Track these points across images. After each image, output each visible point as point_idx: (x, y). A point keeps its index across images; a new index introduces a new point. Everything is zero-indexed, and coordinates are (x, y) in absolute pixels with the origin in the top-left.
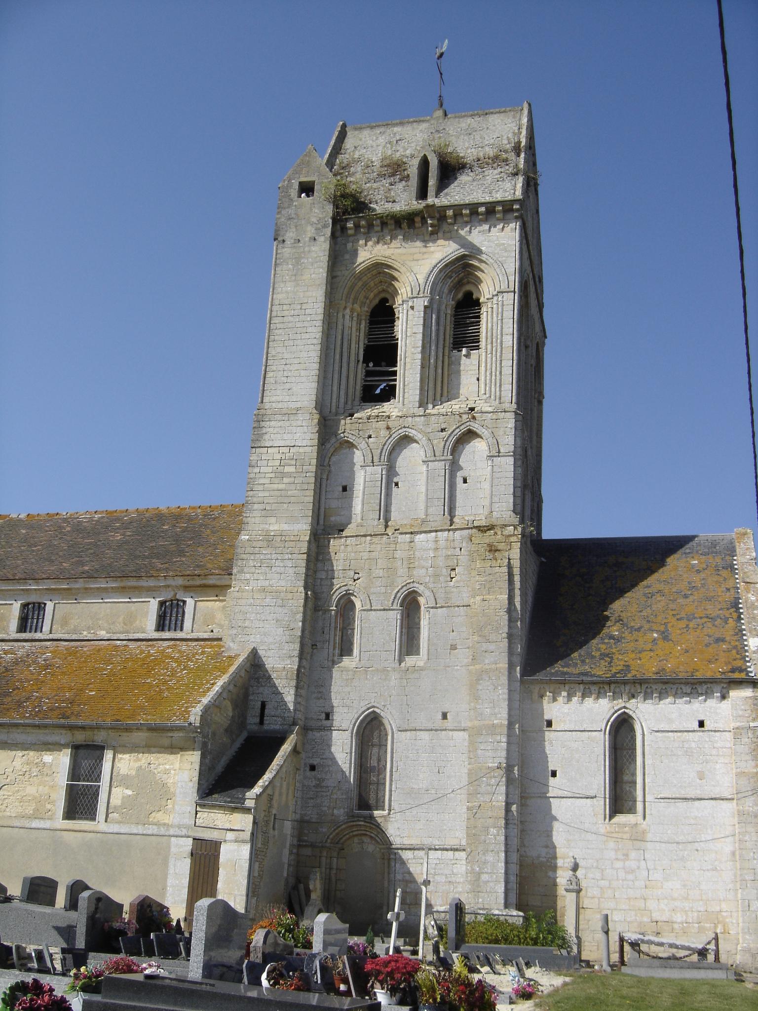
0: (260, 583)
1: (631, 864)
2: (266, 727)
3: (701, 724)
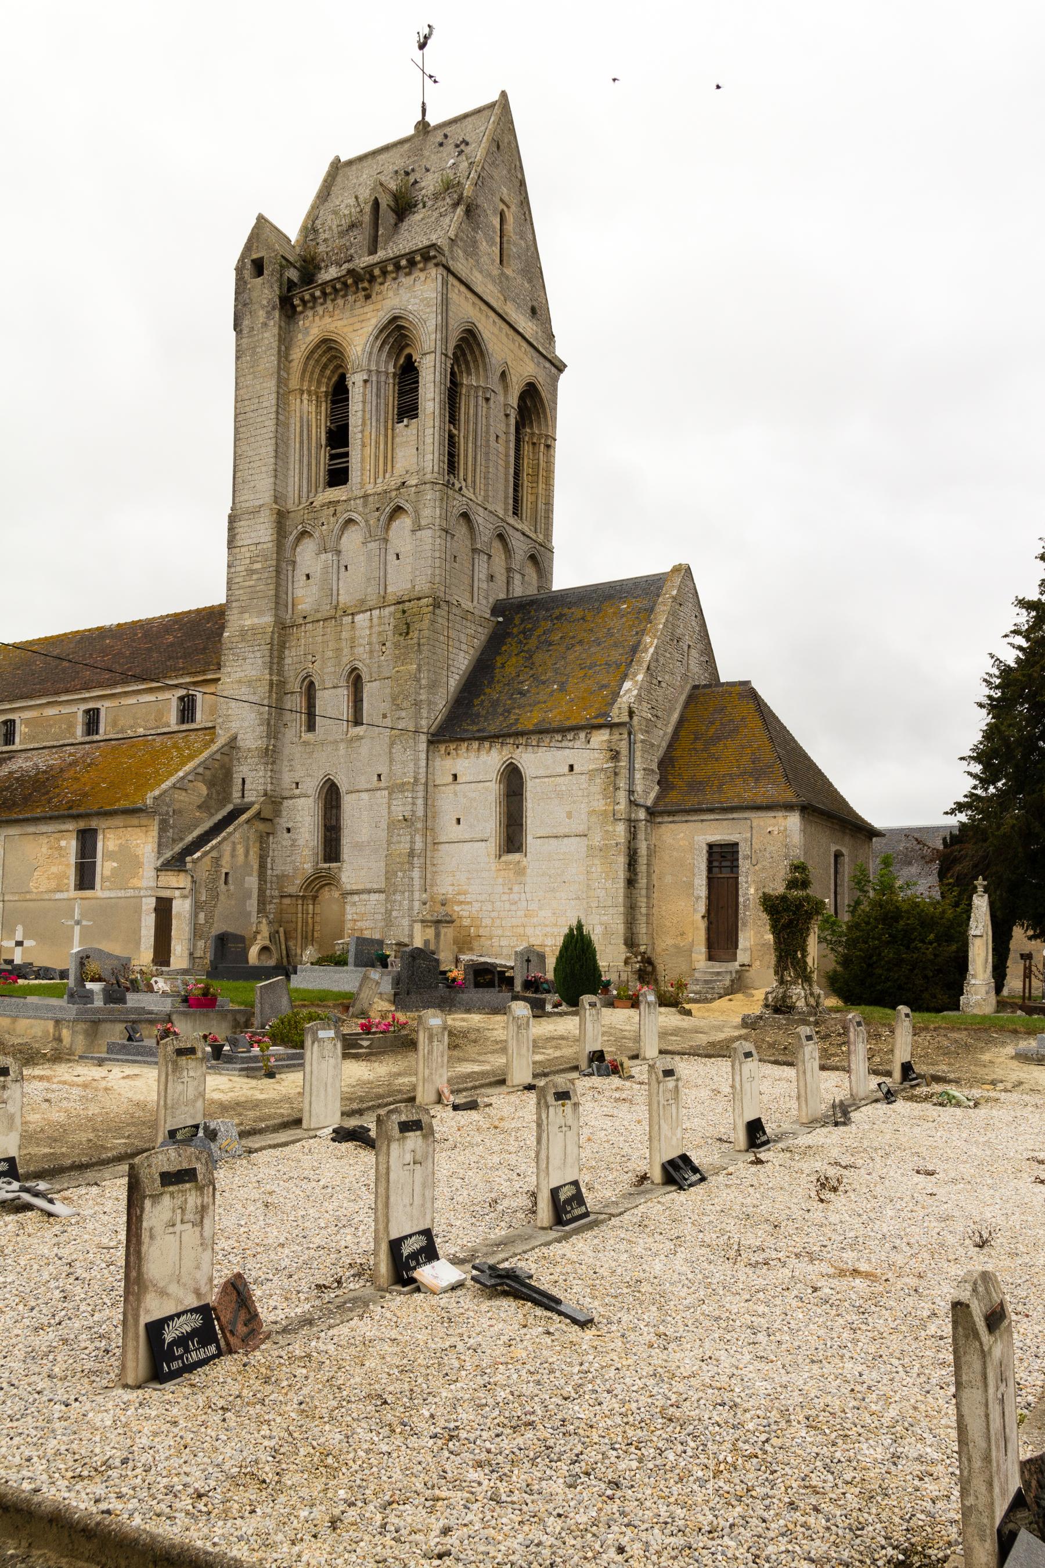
0: (238, 675)
1: (515, 897)
2: (246, 800)
3: (571, 768)
